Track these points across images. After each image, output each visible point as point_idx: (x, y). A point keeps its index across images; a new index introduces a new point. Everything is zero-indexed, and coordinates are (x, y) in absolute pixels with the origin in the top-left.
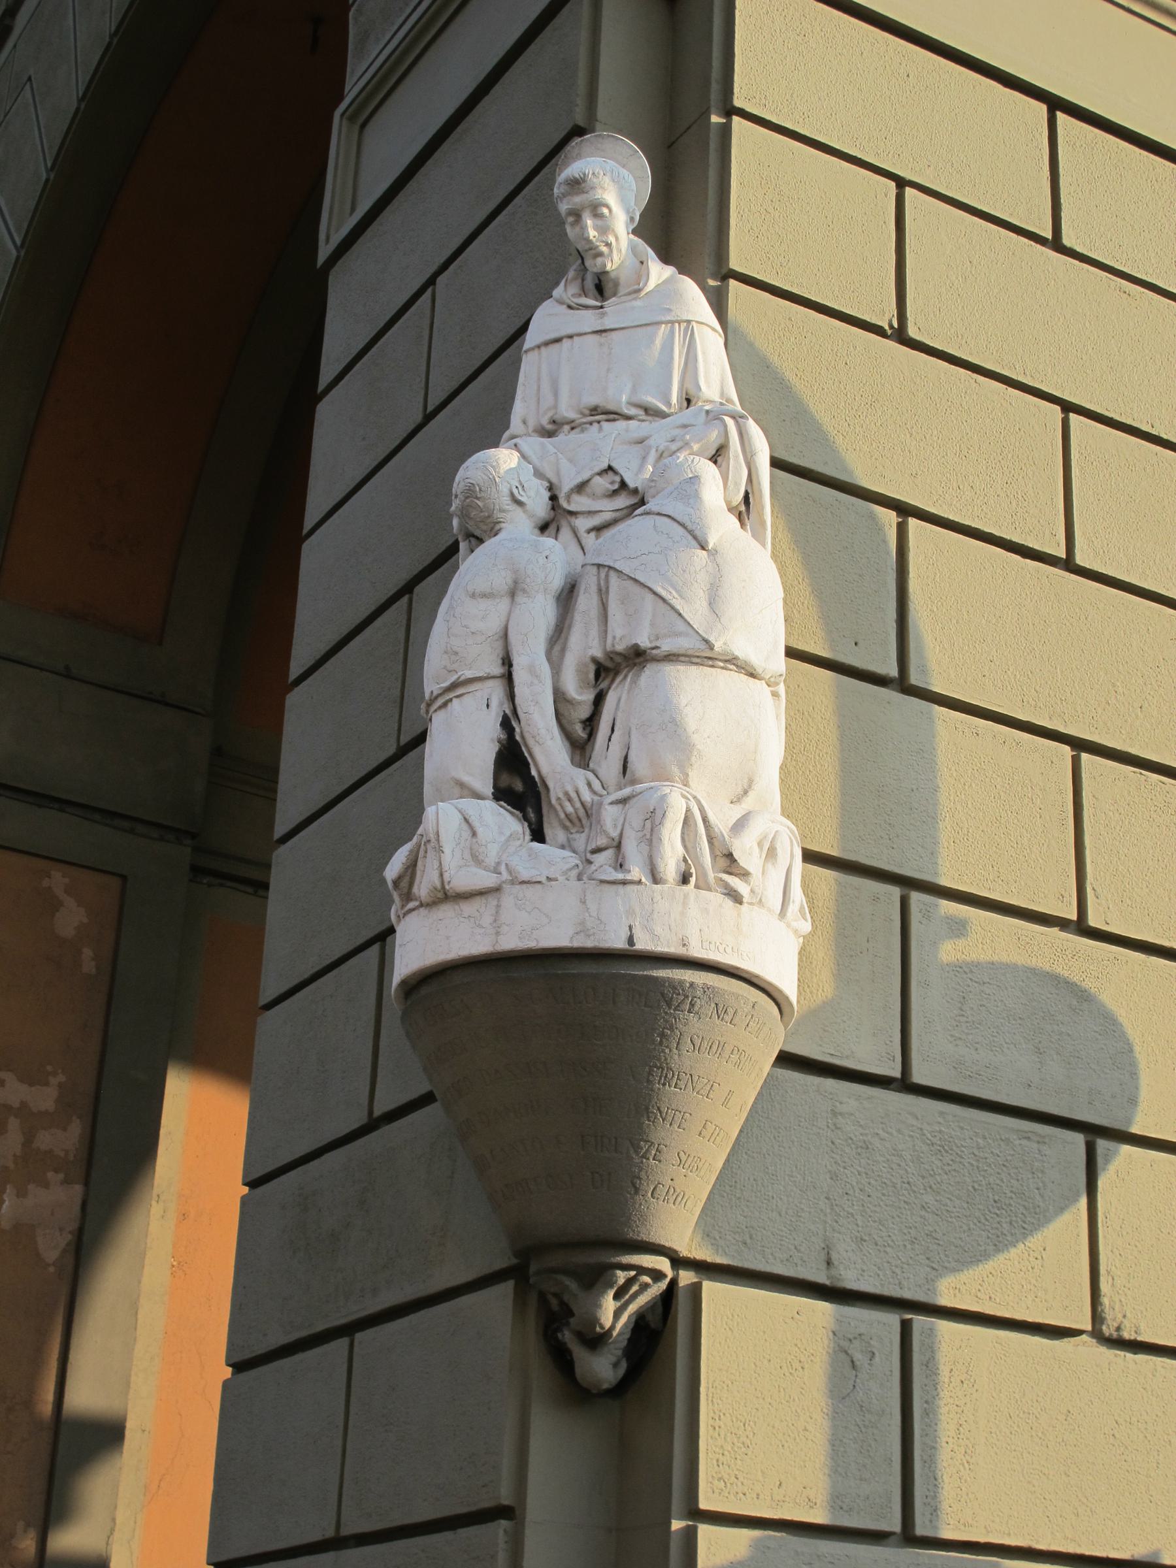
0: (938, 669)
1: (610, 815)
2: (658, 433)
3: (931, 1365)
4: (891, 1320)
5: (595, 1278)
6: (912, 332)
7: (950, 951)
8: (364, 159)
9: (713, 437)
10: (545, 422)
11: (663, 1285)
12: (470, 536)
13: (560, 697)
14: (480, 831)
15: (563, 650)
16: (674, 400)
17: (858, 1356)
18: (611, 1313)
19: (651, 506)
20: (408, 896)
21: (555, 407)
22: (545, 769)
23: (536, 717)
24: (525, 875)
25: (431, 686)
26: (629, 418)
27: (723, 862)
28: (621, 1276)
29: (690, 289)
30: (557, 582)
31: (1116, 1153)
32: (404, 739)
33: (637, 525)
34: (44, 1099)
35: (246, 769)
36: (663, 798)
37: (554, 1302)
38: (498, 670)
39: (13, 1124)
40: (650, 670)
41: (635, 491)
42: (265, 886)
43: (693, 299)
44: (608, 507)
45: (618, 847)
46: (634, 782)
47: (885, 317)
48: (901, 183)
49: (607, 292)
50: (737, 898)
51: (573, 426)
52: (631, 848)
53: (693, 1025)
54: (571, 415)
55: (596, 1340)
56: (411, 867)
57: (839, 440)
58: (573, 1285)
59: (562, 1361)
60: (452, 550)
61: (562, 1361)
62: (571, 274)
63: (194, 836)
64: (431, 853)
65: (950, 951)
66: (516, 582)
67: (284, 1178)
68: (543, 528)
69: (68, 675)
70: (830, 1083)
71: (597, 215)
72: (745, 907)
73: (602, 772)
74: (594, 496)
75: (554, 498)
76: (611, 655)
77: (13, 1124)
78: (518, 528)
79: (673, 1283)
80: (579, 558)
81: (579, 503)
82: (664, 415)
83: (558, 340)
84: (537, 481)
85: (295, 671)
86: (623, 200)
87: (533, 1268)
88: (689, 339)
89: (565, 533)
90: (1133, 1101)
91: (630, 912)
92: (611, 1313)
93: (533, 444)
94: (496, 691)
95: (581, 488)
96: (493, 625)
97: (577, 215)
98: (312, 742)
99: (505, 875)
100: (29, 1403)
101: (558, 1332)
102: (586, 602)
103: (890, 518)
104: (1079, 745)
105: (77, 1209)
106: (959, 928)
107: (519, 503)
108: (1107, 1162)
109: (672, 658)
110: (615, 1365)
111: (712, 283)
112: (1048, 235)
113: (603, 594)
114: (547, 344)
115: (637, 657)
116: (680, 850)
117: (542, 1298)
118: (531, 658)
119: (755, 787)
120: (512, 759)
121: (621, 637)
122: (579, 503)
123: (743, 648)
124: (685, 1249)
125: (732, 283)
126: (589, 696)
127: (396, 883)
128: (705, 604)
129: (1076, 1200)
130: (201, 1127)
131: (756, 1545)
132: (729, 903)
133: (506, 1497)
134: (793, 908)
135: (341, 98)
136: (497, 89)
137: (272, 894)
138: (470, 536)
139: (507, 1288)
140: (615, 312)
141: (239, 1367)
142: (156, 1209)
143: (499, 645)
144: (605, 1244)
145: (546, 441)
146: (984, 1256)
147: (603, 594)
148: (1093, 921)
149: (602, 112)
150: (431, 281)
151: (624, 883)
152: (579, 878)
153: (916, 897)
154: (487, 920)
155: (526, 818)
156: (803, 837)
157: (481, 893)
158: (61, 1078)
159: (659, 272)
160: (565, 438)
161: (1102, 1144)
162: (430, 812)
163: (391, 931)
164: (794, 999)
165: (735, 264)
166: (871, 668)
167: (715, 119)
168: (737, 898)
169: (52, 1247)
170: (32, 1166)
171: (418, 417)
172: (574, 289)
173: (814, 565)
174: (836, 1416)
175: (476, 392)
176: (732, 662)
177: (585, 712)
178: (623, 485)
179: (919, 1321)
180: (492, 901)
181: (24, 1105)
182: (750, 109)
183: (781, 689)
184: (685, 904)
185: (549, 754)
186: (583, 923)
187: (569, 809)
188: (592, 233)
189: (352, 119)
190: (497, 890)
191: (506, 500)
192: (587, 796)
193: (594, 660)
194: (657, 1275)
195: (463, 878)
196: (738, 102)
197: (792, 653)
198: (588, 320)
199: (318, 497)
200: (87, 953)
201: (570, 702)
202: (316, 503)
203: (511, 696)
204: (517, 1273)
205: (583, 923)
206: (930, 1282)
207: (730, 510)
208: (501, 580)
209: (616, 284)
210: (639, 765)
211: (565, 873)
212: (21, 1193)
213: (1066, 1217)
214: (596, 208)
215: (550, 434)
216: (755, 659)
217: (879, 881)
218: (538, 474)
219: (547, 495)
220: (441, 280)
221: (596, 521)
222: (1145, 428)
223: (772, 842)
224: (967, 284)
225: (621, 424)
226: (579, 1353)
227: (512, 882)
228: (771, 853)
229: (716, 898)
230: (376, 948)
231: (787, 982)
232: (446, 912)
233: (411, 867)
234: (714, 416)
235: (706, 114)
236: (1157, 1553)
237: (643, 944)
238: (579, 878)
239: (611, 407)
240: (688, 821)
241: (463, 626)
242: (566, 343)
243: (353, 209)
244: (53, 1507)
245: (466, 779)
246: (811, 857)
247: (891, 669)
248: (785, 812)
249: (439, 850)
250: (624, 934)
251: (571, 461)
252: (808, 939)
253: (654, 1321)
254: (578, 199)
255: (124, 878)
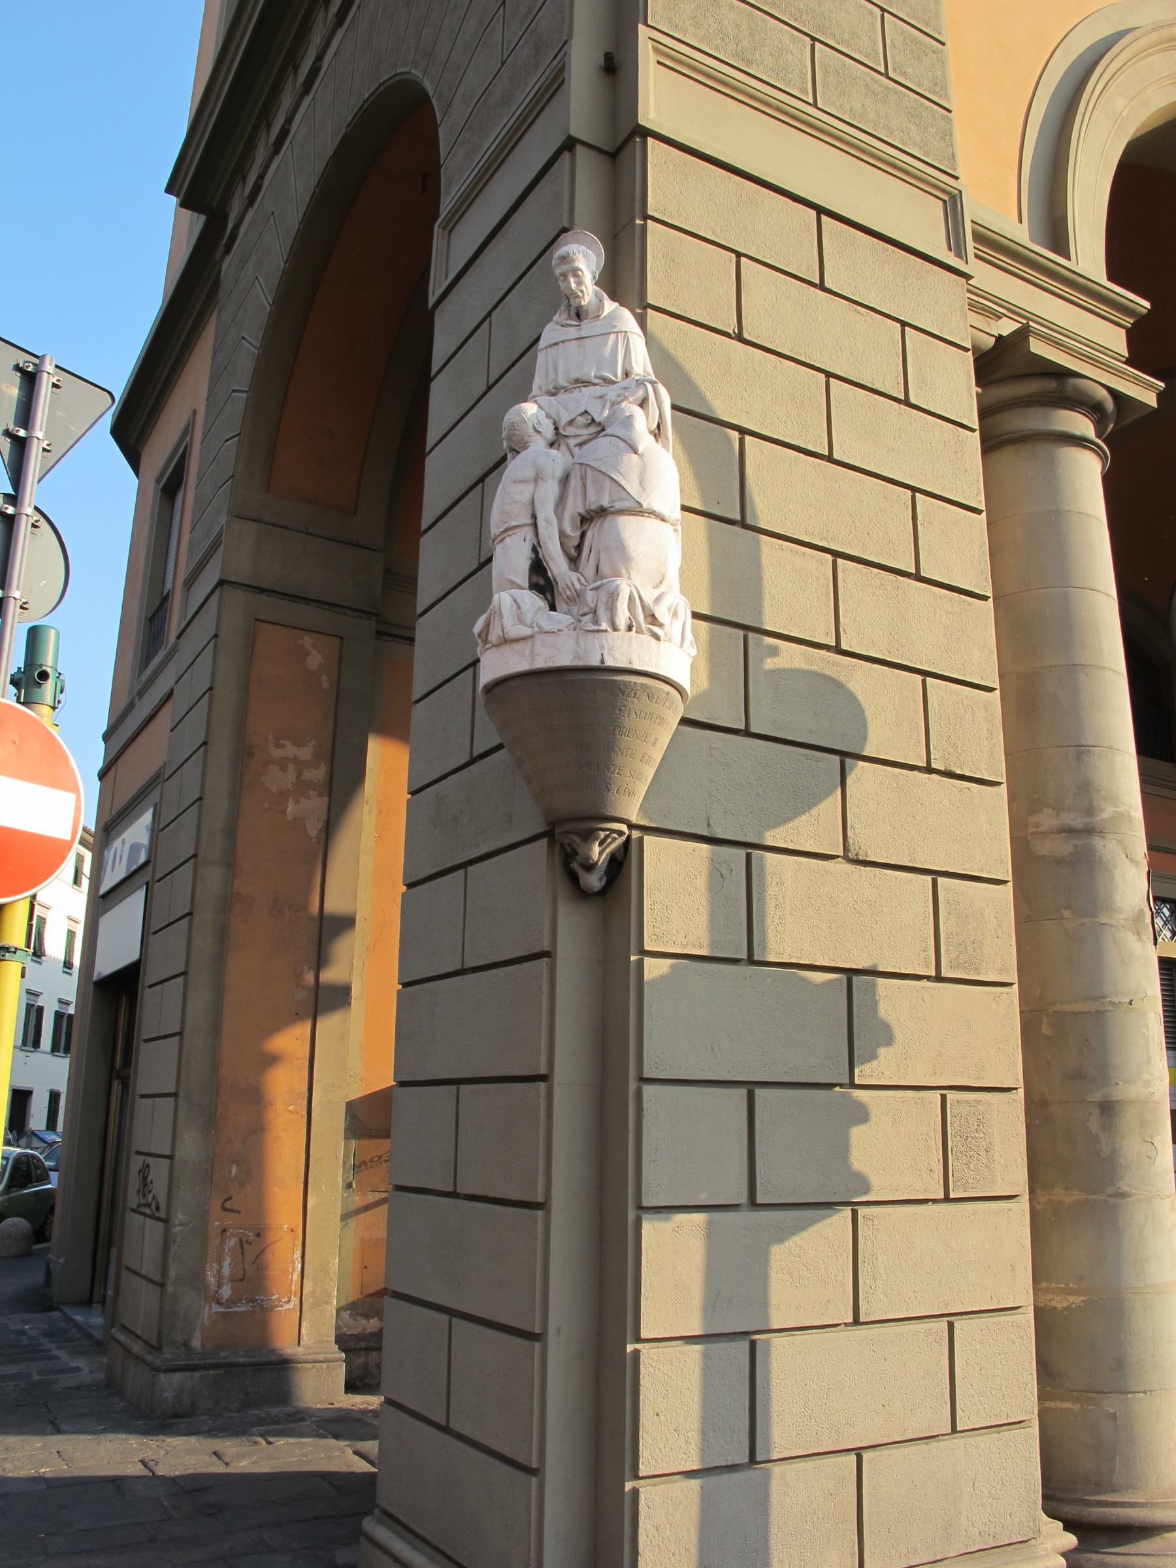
0: (764, 513)
1: (590, 596)
2: (611, 392)
3: (762, 875)
4: (741, 853)
5: (588, 836)
6: (746, 336)
7: (770, 664)
8: (451, 250)
9: (640, 393)
10: (551, 387)
11: (624, 838)
12: (512, 450)
13: (562, 535)
14: (522, 606)
15: (563, 509)
16: (619, 374)
17: (724, 872)
18: (597, 853)
19: (609, 431)
20: (486, 642)
21: (556, 379)
22: (556, 573)
23: (550, 546)
24: (547, 628)
25: (494, 531)
26: (595, 385)
27: (650, 619)
28: (602, 834)
29: (626, 313)
30: (559, 473)
31: (856, 765)
32: (483, 560)
33: (602, 442)
34: (306, 753)
35: (400, 578)
36: (617, 586)
37: (568, 849)
38: (529, 521)
39: (291, 767)
40: (608, 522)
41: (600, 424)
42: (412, 640)
43: (628, 321)
44: (585, 433)
45: (595, 612)
46: (602, 578)
47: (731, 328)
48: (739, 255)
49: (582, 316)
50: (657, 638)
51: (566, 390)
52: (602, 613)
53: (634, 704)
54: (564, 384)
55: (590, 867)
56: (487, 625)
57: (708, 394)
58: (577, 839)
59: (573, 878)
60: (503, 459)
61: (573, 878)
62: (563, 308)
63: (377, 615)
64: (497, 619)
65: (770, 664)
66: (537, 474)
67: (429, 790)
68: (552, 445)
69: (307, 533)
70: (708, 733)
71: (576, 276)
72: (662, 643)
73: (585, 574)
74: (577, 427)
75: (556, 429)
76: (588, 512)
77: (291, 767)
78: (538, 445)
79: (629, 837)
80: (570, 460)
81: (571, 431)
82: (614, 383)
83: (556, 344)
84: (547, 420)
85: (424, 526)
86: (589, 267)
87: (557, 831)
88: (630, 344)
89: (563, 447)
90: (865, 739)
91: (602, 647)
92: (597, 853)
93: (545, 400)
94: (528, 532)
95: (571, 422)
96: (526, 497)
97: (565, 276)
98: (434, 563)
99: (536, 629)
100: (306, 907)
101: (570, 866)
102: (575, 483)
103: (735, 435)
104: (836, 554)
105: (325, 809)
106: (774, 652)
107: (539, 432)
108: (851, 770)
109: (621, 512)
110: (600, 879)
111: (638, 311)
112: (817, 282)
113: (583, 478)
114: (550, 346)
115: (602, 512)
116: (627, 614)
117: (562, 846)
118: (546, 513)
119: (667, 579)
120: (538, 567)
121: (594, 501)
122: (571, 431)
123: (657, 507)
124: (634, 818)
125: (649, 311)
126: (578, 534)
127: (479, 635)
128: (637, 481)
129: (835, 789)
130: (386, 765)
131: (672, 967)
132: (653, 640)
133: (546, 946)
134: (687, 642)
135: (438, 216)
136: (521, 209)
137: (416, 643)
138: (512, 450)
139: (544, 842)
140: (587, 328)
141: (410, 886)
142: (366, 808)
143: (529, 508)
144: (591, 819)
145: (552, 398)
146: (789, 820)
147: (583, 478)
148: (844, 646)
149: (577, 220)
150: (489, 314)
151: (599, 631)
152: (575, 629)
153: (751, 635)
154: (527, 652)
155: (546, 599)
156: (692, 605)
157: (523, 639)
158: (314, 743)
159: (609, 306)
160: (561, 396)
161: (848, 761)
162: (496, 596)
163: (478, 660)
164: (688, 690)
165: (650, 301)
166: (728, 515)
167: (638, 222)
168: (657, 638)
169: (314, 828)
170: (302, 788)
171: (483, 388)
172: (564, 316)
173: (696, 460)
174: (712, 902)
175: (514, 373)
176: (652, 513)
177: (576, 542)
178: (593, 420)
179: (756, 853)
180: (529, 642)
181: (295, 757)
182: (656, 215)
183: (679, 527)
184: (630, 642)
185: (558, 565)
186: (577, 653)
187: (569, 593)
188: (573, 286)
189: (444, 228)
190: (532, 637)
191: (531, 430)
192: (578, 586)
193: (580, 514)
194: (621, 833)
195: (515, 631)
196: (650, 213)
197: (684, 508)
198: (572, 333)
199: (433, 433)
200: (324, 678)
201: (567, 537)
202: (432, 436)
203: (537, 534)
204: (549, 834)
205: (577, 653)
206: (761, 834)
207: (651, 432)
208: (529, 473)
209: (587, 312)
210: (605, 569)
211: (567, 627)
212: (297, 802)
213: (830, 799)
214: (575, 272)
215: (554, 395)
216: (665, 512)
217: (734, 626)
218: (548, 416)
219: (552, 427)
220: (494, 313)
221: (579, 440)
222: (870, 385)
223: (676, 607)
224: (774, 308)
225: (591, 388)
226: (582, 874)
227: (540, 632)
228: (675, 614)
229: (647, 638)
230: (471, 670)
231: (685, 681)
232: (506, 649)
233: (487, 625)
234: (640, 383)
235: (633, 219)
236: (875, 965)
237: (609, 662)
238: (575, 629)
239: (586, 379)
240: (631, 598)
241: (511, 496)
242: (561, 345)
243: (446, 277)
244: (320, 960)
245: (514, 579)
246: (696, 616)
247: (737, 516)
248: (682, 592)
249: (501, 616)
250: (599, 658)
251: (565, 408)
252: (695, 658)
253: (620, 857)
254: (565, 267)
255: (341, 638)
